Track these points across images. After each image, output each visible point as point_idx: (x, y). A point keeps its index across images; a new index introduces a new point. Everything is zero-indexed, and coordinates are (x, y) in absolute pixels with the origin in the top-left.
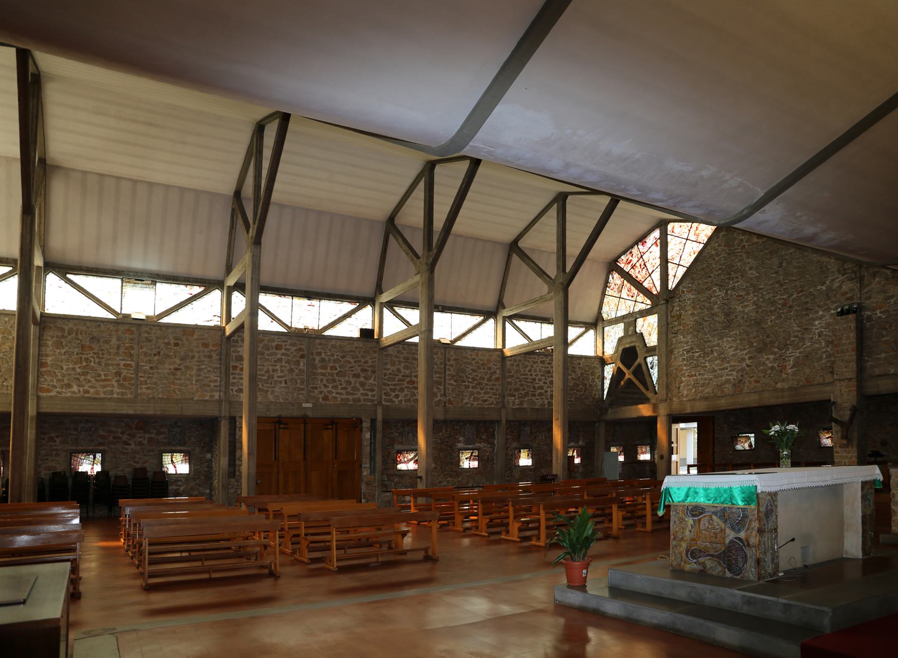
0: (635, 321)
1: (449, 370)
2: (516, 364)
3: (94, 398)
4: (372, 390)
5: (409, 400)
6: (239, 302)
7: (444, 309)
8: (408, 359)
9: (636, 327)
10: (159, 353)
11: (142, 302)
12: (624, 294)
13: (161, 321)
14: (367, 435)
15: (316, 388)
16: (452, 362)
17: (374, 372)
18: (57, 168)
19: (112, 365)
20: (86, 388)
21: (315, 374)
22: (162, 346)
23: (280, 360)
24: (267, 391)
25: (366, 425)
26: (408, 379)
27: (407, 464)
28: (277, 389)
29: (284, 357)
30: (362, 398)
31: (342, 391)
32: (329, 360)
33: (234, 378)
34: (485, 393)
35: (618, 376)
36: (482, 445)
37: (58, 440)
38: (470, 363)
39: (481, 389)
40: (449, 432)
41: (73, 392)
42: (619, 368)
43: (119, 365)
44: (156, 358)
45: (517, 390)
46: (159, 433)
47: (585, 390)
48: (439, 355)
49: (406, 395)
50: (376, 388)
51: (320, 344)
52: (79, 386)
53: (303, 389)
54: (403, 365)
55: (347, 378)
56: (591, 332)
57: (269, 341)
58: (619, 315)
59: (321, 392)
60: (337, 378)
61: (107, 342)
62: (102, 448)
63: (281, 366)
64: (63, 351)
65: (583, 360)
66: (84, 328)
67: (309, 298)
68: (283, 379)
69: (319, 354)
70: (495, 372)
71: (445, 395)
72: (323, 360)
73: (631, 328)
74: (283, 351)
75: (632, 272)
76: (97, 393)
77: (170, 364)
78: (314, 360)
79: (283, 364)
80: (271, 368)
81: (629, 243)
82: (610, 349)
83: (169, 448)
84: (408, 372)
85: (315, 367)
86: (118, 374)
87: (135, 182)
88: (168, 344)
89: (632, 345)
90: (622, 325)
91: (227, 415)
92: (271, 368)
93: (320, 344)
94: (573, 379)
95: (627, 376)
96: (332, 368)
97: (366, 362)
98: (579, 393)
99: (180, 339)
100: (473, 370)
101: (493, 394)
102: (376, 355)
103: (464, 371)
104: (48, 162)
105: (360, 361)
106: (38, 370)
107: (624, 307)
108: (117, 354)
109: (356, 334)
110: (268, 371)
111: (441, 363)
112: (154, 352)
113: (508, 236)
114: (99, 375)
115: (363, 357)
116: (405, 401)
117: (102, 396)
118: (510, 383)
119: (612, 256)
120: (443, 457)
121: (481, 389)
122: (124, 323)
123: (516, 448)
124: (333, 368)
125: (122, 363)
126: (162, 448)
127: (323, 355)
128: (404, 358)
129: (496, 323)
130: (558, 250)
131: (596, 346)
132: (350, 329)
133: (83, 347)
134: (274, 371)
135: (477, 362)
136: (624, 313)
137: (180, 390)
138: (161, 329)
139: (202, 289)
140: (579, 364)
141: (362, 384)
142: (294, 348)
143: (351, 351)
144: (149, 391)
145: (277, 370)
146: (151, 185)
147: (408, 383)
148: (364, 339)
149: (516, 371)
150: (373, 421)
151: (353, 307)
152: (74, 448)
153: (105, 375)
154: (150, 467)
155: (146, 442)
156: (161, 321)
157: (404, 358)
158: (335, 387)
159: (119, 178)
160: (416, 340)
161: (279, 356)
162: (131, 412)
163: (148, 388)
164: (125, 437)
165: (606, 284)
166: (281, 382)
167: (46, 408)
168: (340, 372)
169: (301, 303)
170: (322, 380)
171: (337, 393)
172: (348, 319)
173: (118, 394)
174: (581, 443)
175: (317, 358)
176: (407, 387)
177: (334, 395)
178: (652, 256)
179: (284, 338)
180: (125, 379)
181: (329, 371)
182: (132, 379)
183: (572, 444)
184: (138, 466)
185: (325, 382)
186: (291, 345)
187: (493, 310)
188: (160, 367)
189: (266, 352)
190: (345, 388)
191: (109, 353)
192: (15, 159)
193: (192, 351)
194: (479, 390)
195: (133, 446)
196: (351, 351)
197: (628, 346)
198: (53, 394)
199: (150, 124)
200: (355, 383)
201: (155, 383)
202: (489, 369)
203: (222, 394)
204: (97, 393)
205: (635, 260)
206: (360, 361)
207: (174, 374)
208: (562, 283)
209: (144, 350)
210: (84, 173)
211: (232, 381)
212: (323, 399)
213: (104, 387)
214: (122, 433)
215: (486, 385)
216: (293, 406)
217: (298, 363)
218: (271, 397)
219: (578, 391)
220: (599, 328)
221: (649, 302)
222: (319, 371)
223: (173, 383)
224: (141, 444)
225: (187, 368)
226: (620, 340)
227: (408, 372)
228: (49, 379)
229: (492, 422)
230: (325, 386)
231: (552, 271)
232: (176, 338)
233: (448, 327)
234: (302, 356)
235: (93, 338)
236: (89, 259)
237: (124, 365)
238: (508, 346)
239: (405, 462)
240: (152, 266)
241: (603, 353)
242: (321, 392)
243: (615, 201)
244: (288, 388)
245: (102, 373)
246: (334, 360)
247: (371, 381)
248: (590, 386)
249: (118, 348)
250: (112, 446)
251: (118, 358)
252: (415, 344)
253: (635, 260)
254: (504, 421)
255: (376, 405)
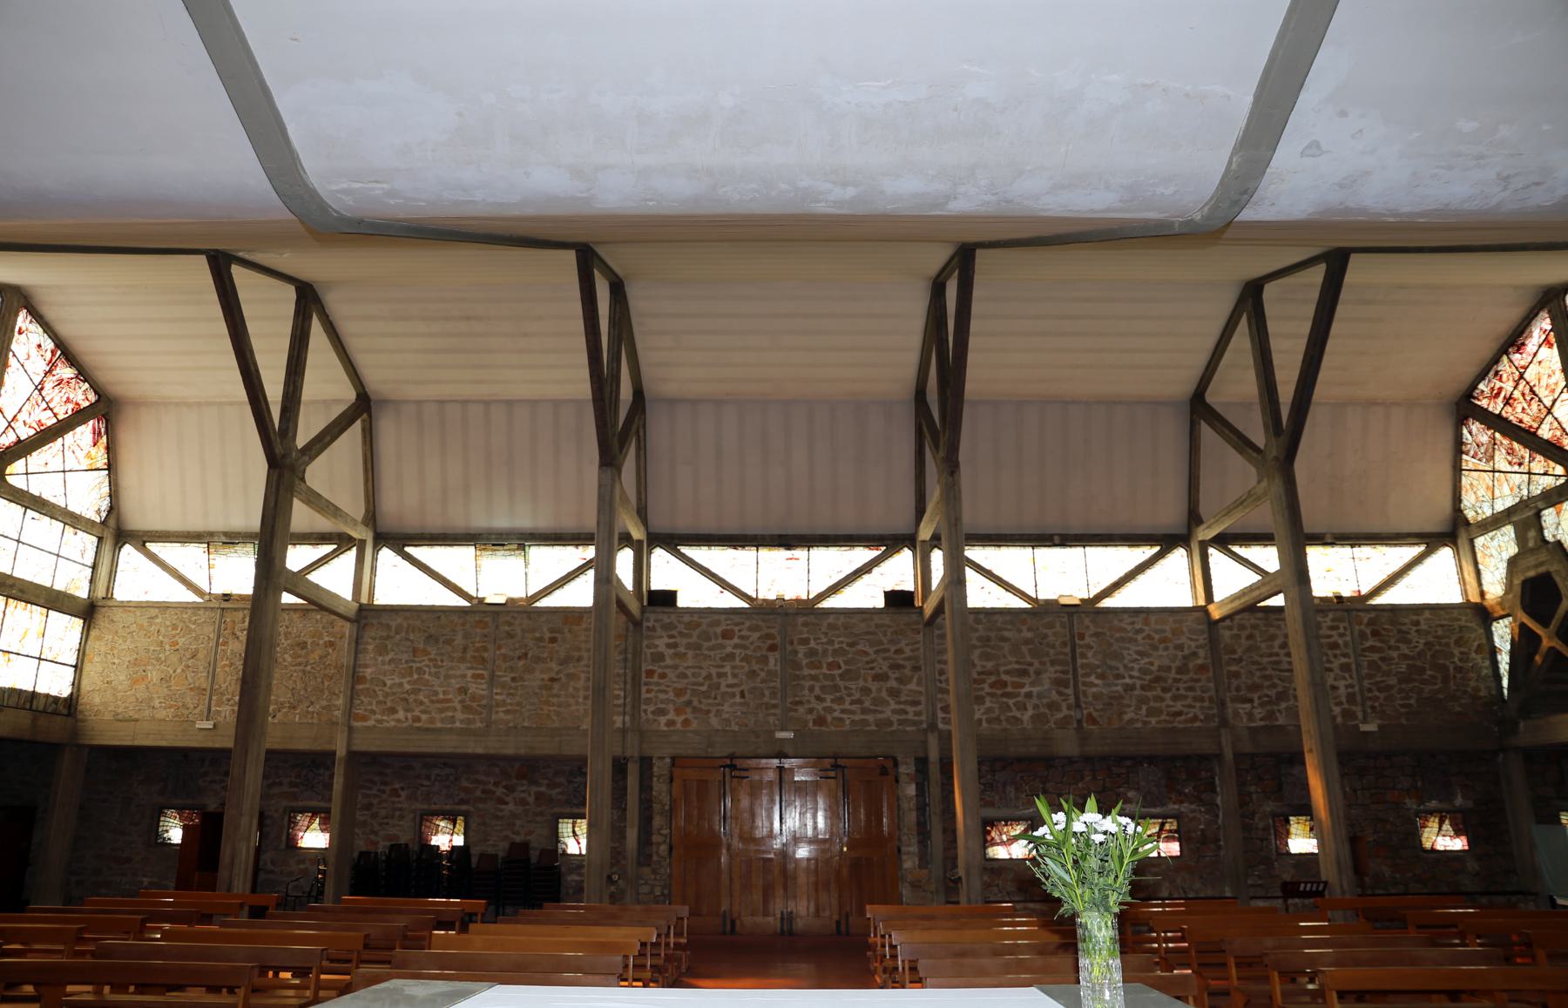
0: (1538, 516)
1: (1083, 656)
2: (1244, 634)
3: (427, 729)
4: (915, 703)
5: (998, 720)
6: (624, 562)
7: (1320, 540)
8: (988, 639)
9: (1541, 529)
10: (526, 655)
11: (501, 578)
12: (1501, 462)
13: (538, 604)
14: (911, 790)
15: (801, 703)
16: (1088, 640)
17: (916, 669)
18: (138, 403)
19: (455, 677)
20: (417, 713)
21: (797, 677)
22: (531, 643)
23: (731, 657)
24: (709, 712)
25: (907, 769)
26: (993, 679)
27: (1301, 843)
28: (726, 708)
29: (737, 651)
30: (894, 718)
31: (853, 707)
32: (825, 651)
33: (648, 691)
34: (1175, 698)
35: (1524, 643)
36: (1185, 808)
37: (403, 794)
38: (1131, 640)
39: (1164, 690)
40: (1382, 784)
41: (399, 721)
42: (1522, 626)
43: (464, 676)
44: (521, 663)
45: (1255, 687)
46: (551, 786)
47: (1446, 680)
48: (1058, 628)
49: (989, 710)
50: (923, 699)
51: (805, 624)
52: (407, 710)
53: (775, 706)
54: (977, 652)
55: (861, 683)
56: (1445, 554)
57: (711, 625)
58: (1500, 506)
59: (811, 711)
60: (841, 684)
61: (449, 642)
62: (464, 807)
63: (733, 667)
64: (387, 658)
65: (1427, 614)
66: (418, 623)
67: (789, 547)
68: (737, 690)
69: (805, 642)
70: (1194, 654)
71: (1078, 705)
72: (812, 653)
73: (1532, 534)
74: (736, 640)
75: (1508, 413)
76: (432, 720)
77: (542, 672)
78: (796, 652)
79: (737, 662)
80: (714, 671)
81: (1487, 352)
82: (1494, 585)
83: (568, 810)
84: (990, 665)
85: (798, 666)
86: (463, 690)
87: (487, 403)
88: (540, 639)
89: (1542, 570)
90: (1509, 530)
91: (636, 755)
92: (714, 671)
93: (805, 624)
94: (1405, 657)
95: (1546, 643)
96: (831, 666)
97: (898, 652)
98: (1427, 688)
99: (560, 631)
100: (1139, 653)
101: (1195, 699)
102: (920, 637)
103: (1118, 656)
104: (372, 397)
105: (887, 650)
106: (353, 688)
107: (1506, 490)
108: (462, 660)
109: (880, 603)
110: (709, 677)
111: (1064, 644)
112: (518, 653)
113: (1181, 383)
114: (436, 693)
115: (892, 642)
116: (989, 721)
117: (439, 725)
118: (1236, 675)
119: (1455, 387)
120: (1375, 839)
121: (1164, 690)
122: (480, 614)
123: (1274, 815)
124: (831, 666)
125: (470, 673)
126: (557, 810)
127: (812, 644)
128: (980, 639)
129: (1190, 555)
130: (1261, 395)
131: (1463, 581)
132: (867, 595)
133: (415, 651)
134: (720, 675)
135: (1149, 637)
136: (1510, 502)
137: (558, 714)
138: (529, 618)
139: (1422, 548)
140: (1417, 623)
141: (894, 693)
142: (757, 635)
143: (868, 633)
144: (509, 717)
145: (724, 675)
146: (510, 403)
147: (992, 686)
148: (892, 610)
149: (1249, 649)
150: (922, 763)
151: (874, 553)
152: (425, 807)
153: (445, 693)
154: (537, 841)
155: (531, 799)
156: (538, 604)
157: (980, 639)
158: (840, 700)
159: (465, 402)
160: (1278, 601)
161: (729, 650)
162: (480, 751)
163: (507, 712)
164: (499, 791)
165: (1459, 448)
166: (734, 695)
167: (360, 746)
168: (847, 671)
169: (773, 558)
170: (811, 689)
171: (843, 711)
172: (866, 577)
173: (461, 721)
174: (1459, 801)
175: (802, 649)
176: (992, 695)
177: (836, 714)
178: (1544, 370)
179: (737, 619)
180: (473, 698)
181: (825, 670)
182: (483, 697)
183: (1434, 804)
184: (518, 839)
185: (817, 691)
186: (751, 629)
187: (1183, 531)
188: (527, 676)
189: (706, 644)
190: (859, 702)
191: (452, 659)
192: (241, 403)
193: (579, 649)
194: (1159, 692)
195: (511, 807)
196: (868, 633)
197: (1531, 574)
198: (371, 723)
199: (468, 318)
200: (879, 690)
201: (519, 704)
202: (1180, 647)
203: (627, 718)
204: (432, 720)
205: (1508, 387)
206: (887, 650)
207: (549, 688)
208: (1276, 458)
209: (503, 651)
210: (419, 403)
211: (644, 695)
212: (815, 722)
213: (441, 711)
214: (496, 784)
215: (1175, 680)
216: (757, 736)
217: (765, 660)
218: (714, 722)
219: (1424, 682)
220: (1462, 541)
221: (1560, 470)
222: (806, 672)
223: (548, 703)
224: (523, 802)
225: (571, 677)
226: (1512, 563)
227: (990, 665)
228: (366, 700)
229: (1204, 758)
230: (818, 698)
231: (1258, 437)
232: (552, 631)
233: (1337, 572)
234: (772, 648)
235: (430, 636)
236: (434, 523)
237: (474, 676)
238: (1218, 596)
239: (1002, 843)
240: (524, 520)
241: (1482, 594)
242: (811, 711)
243: (1336, 262)
244: (746, 704)
245: (440, 690)
246: (835, 651)
247: (913, 686)
248: (1459, 669)
249: (465, 649)
250: (481, 806)
251: (463, 666)
252: (1279, 610)
253: (1508, 387)
254: (1228, 755)
255: (925, 731)
